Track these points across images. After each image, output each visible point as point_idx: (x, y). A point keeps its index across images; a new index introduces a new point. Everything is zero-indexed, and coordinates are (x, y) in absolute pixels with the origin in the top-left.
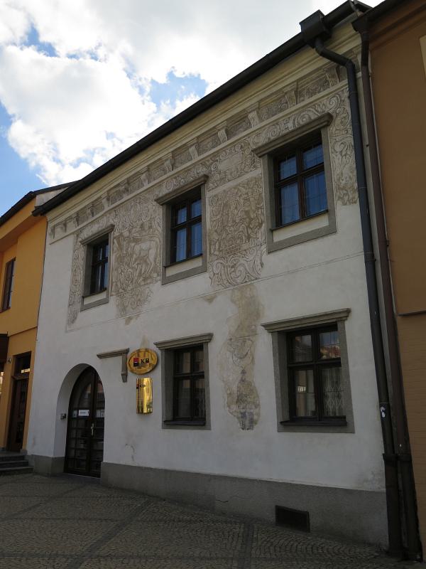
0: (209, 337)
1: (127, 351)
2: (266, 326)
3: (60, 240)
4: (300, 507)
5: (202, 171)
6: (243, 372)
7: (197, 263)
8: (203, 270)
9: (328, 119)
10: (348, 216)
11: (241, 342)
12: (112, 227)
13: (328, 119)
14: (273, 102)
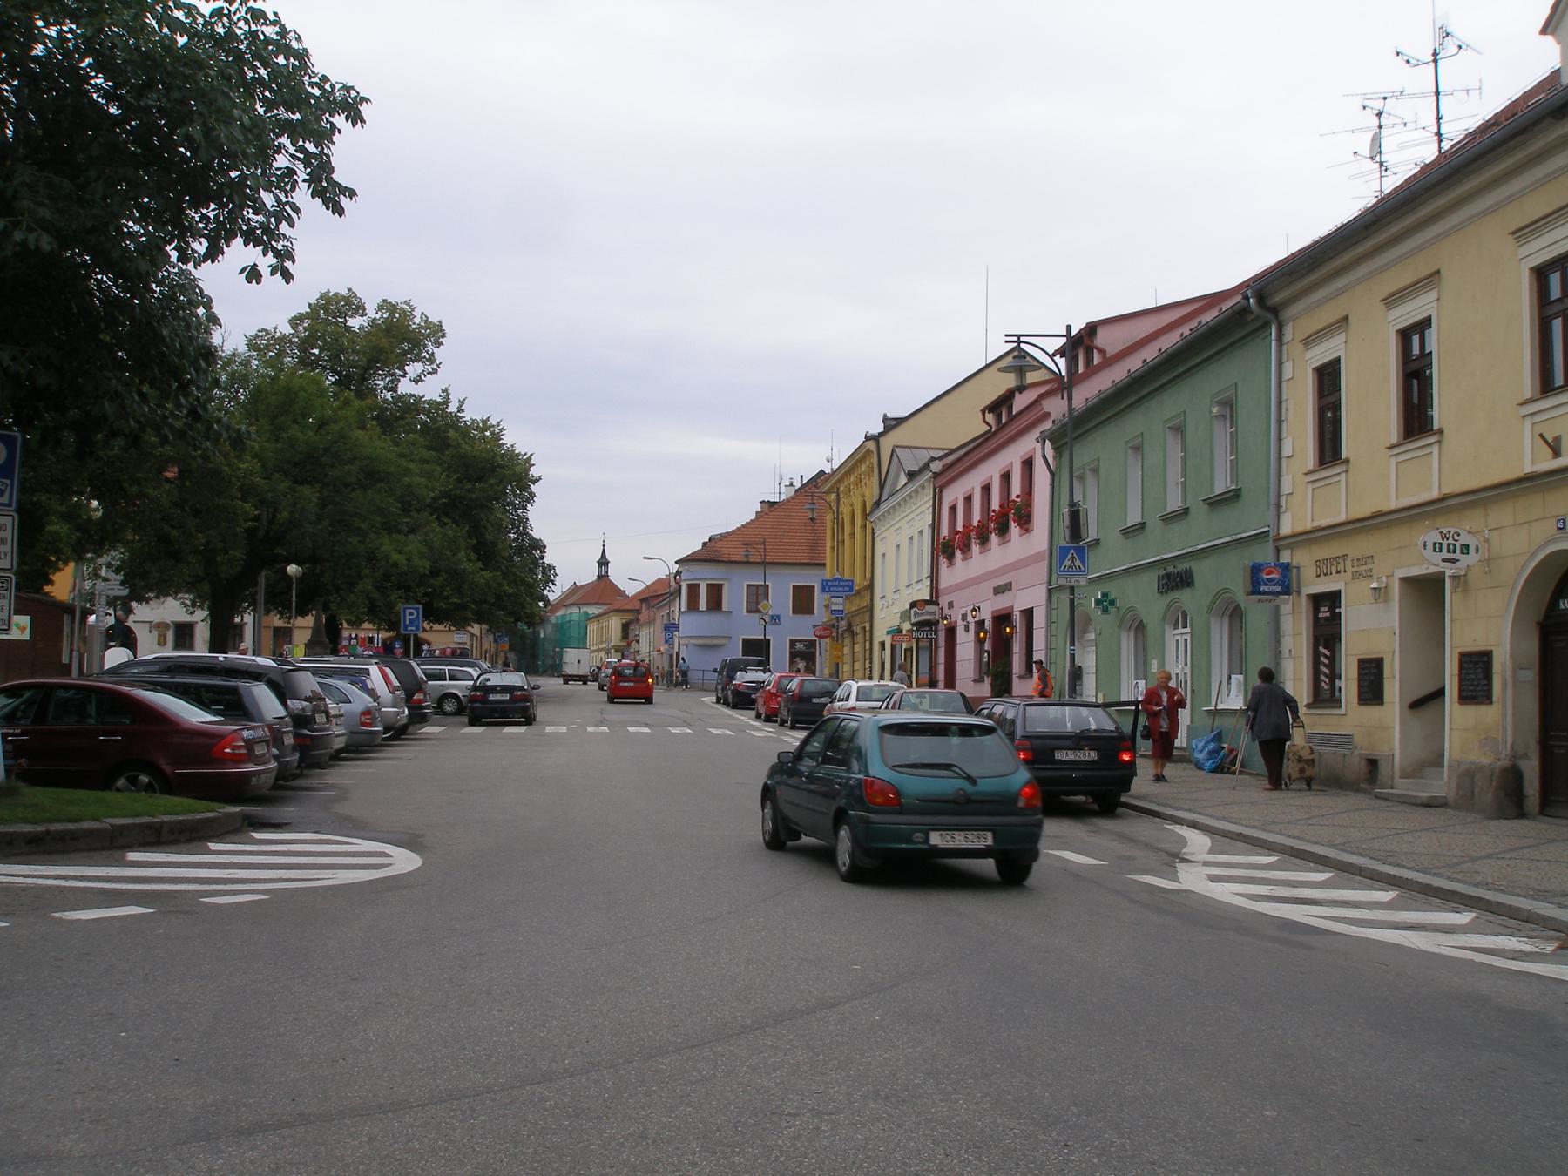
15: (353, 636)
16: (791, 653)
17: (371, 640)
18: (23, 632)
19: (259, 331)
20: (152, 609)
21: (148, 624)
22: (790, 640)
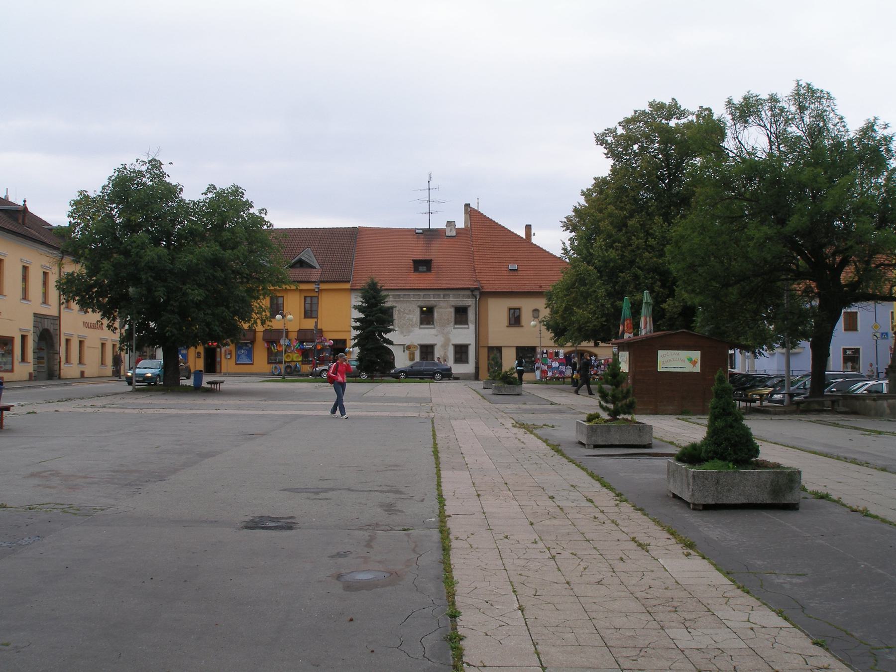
0: (436, 344)
1: (405, 345)
2: (453, 345)
3: (103, 377)
4: (458, 376)
5: (434, 303)
6: (445, 352)
7: (433, 326)
8: (434, 328)
9: (469, 306)
10: (472, 326)
11: (445, 346)
12: (396, 307)
13: (469, 306)
14: (100, 509)
15: (545, 351)
16: (844, 357)
17: (557, 354)
18: (694, 365)
19: (605, 130)
20: (405, 336)
21: (402, 347)
22: (843, 349)
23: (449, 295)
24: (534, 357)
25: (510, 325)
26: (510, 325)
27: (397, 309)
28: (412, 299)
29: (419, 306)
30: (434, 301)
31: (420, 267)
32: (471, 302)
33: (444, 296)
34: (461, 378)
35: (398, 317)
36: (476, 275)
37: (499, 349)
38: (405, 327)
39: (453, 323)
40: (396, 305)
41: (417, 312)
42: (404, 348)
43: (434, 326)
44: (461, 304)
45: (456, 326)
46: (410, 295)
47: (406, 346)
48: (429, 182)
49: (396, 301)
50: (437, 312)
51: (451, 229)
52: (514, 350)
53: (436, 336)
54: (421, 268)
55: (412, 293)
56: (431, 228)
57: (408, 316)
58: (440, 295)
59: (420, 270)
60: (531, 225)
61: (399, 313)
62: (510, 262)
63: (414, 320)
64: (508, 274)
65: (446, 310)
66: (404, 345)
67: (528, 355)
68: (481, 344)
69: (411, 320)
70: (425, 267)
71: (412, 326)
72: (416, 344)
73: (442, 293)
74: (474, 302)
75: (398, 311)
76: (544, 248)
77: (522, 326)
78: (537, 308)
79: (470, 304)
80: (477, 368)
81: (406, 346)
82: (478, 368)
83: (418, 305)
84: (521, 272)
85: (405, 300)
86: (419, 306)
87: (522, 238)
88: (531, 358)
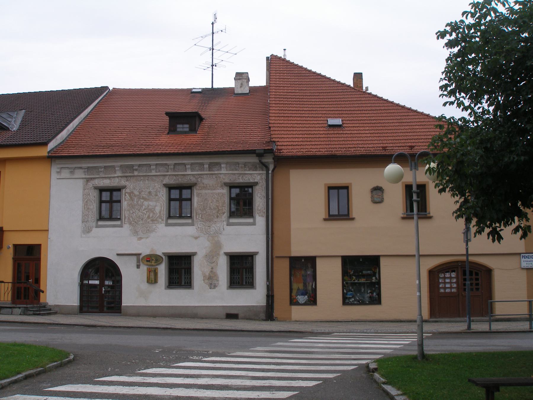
0: (195, 254)
1: (140, 254)
2: (226, 254)
5: (193, 180)
6: (212, 268)
7: (189, 221)
8: (192, 224)
9: (256, 184)
10: (260, 220)
11: (211, 257)
12: (125, 187)
20: (140, 239)
21: (135, 258)
23: (219, 164)
24: (374, 275)
25: (361, 74)
26: (361, 74)
27: (128, 190)
28: (154, 173)
29: (165, 185)
30: (193, 175)
31: (179, 126)
32: (259, 177)
33: (211, 166)
34: (240, 316)
35: (129, 205)
36: (270, 127)
37: (311, 261)
38: (141, 222)
39: (226, 215)
40: (127, 183)
41: (163, 194)
42: (138, 261)
43: (193, 221)
44: (241, 180)
45: (233, 220)
46: (150, 165)
47: (141, 257)
48: (213, 24)
49: (126, 177)
50: (198, 195)
51: (242, 84)
52: (338, 265)
53: (196, 238)
54: (180, 127)
55: (153, 161)
56: (214, 87)
57: (146, 203)
58: (202, 164)
59: (178, 130)
60: (362, 73)
61: (132, 199)
62: (330, 115)
63: (158, 209)
64: (325, 132)
65: (214, 191)
66: (138, 255)
67: (364, 272)
68: (277, 253)
69: (152, 210)
70: (187, 126)
71: (152, 220)
72: (159, 253)
73: (206, 161)
74: (264, 177)
75: (130, 194)
76: (384, 98)
77: (353, 219)
78: (380, 185)
79: (256, 181)
80: (270, 297)
81: (141, 257)
82: (273, 296)
83: (164, 183)
84: (348, 129)
85: (141, 174)
86: (165, 185)
87: (349, 86)
88: (369, 276)
